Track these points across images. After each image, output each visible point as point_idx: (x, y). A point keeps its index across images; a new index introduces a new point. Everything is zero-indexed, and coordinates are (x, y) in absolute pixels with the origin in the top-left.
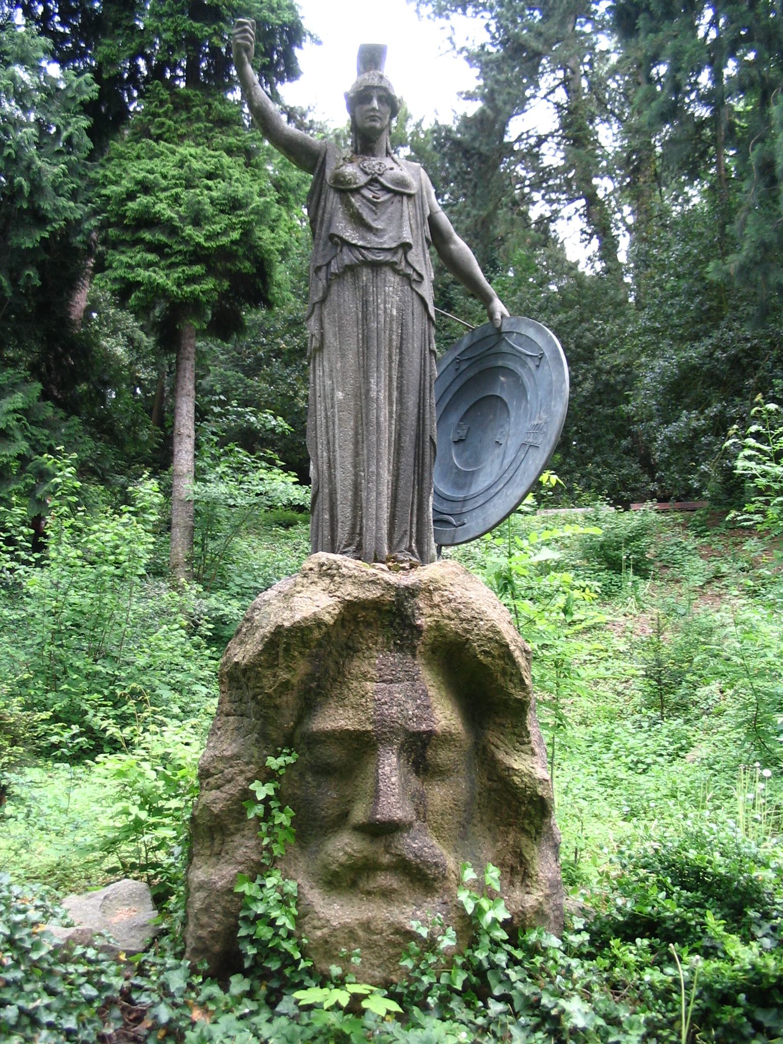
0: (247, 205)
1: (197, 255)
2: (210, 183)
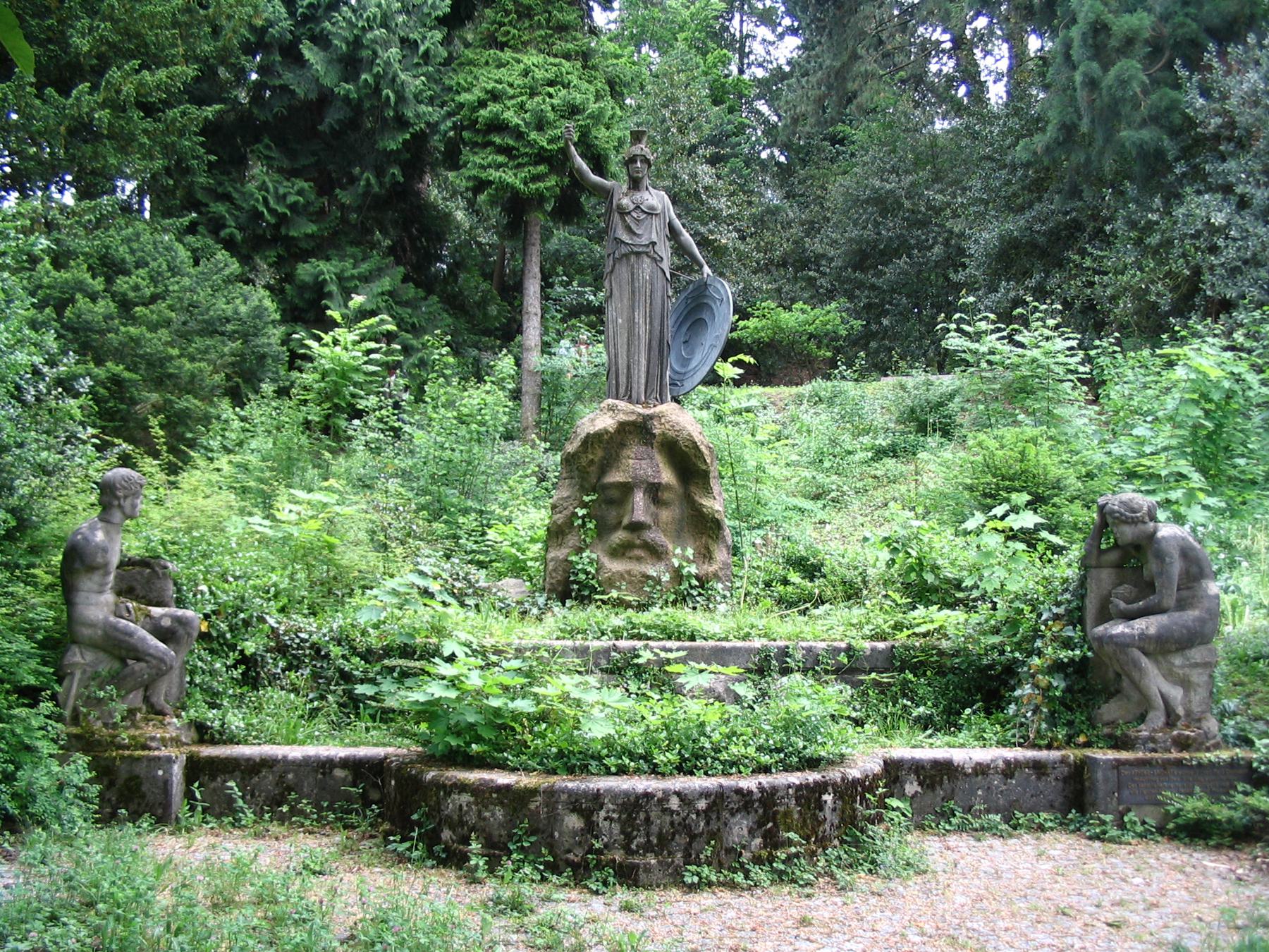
0: (584, 110)
1: (541, 157)
2: (551, 90)
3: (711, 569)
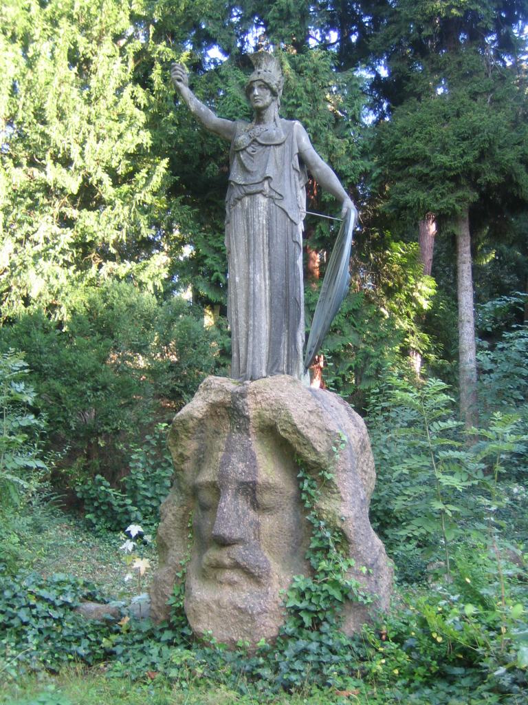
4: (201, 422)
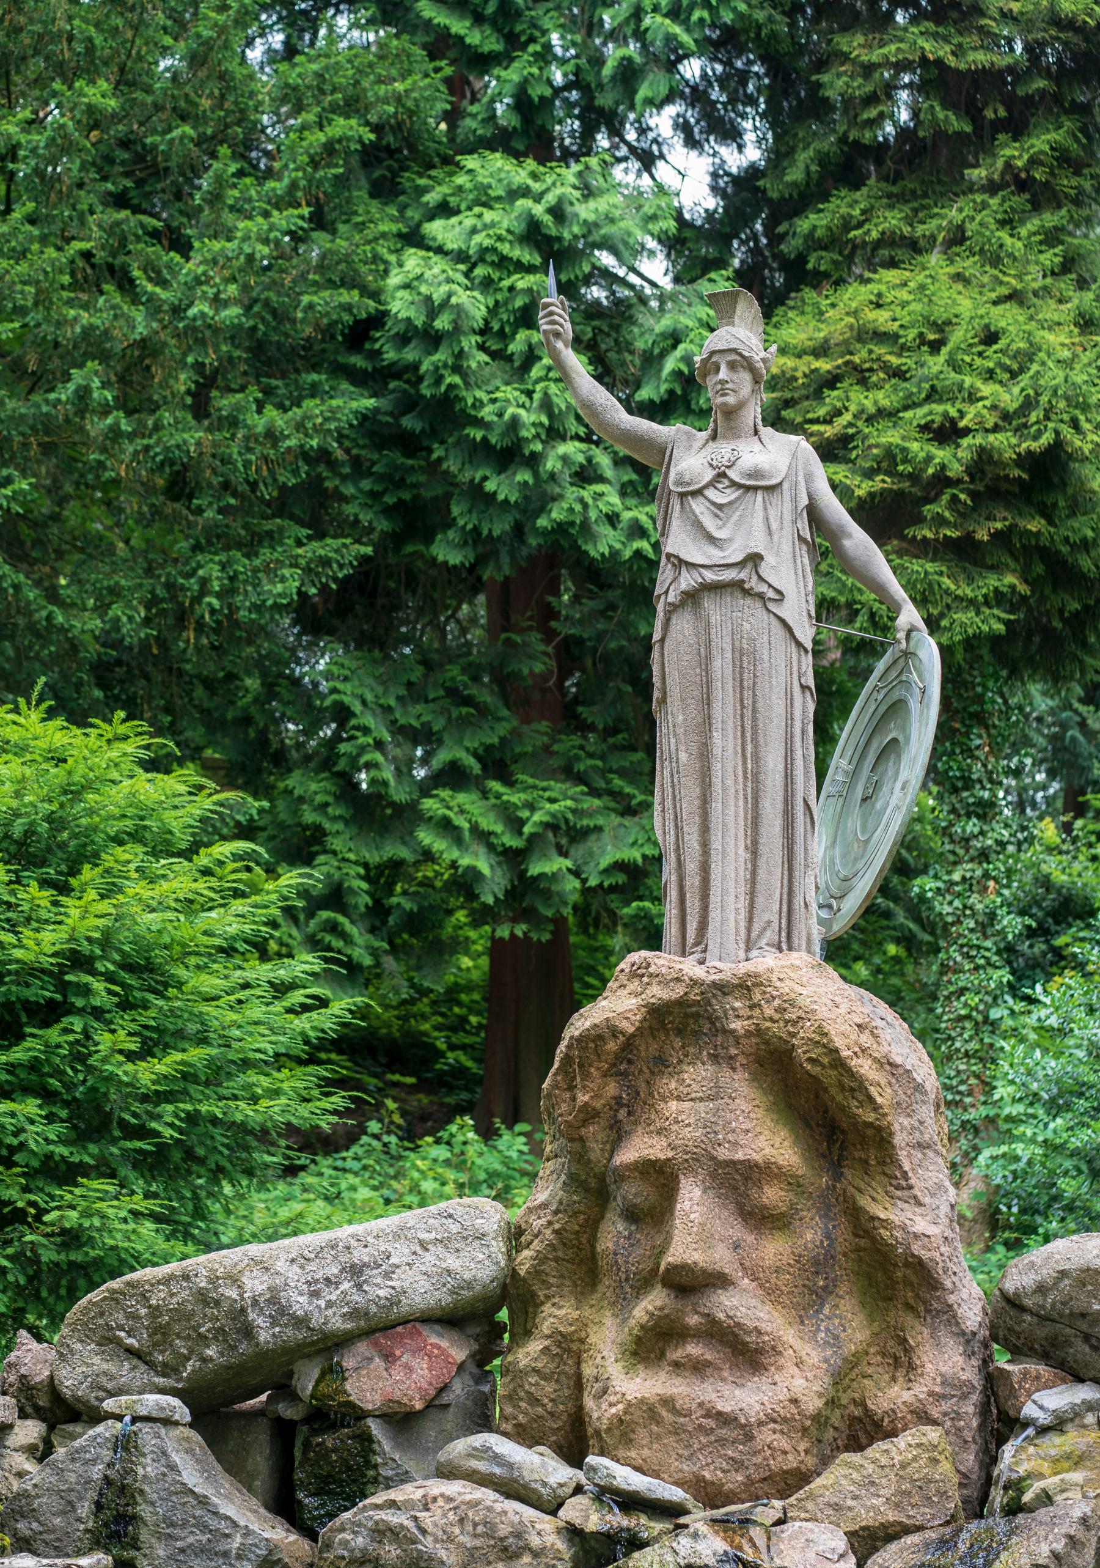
3: (907, 1396)
4: (630, 1043)
